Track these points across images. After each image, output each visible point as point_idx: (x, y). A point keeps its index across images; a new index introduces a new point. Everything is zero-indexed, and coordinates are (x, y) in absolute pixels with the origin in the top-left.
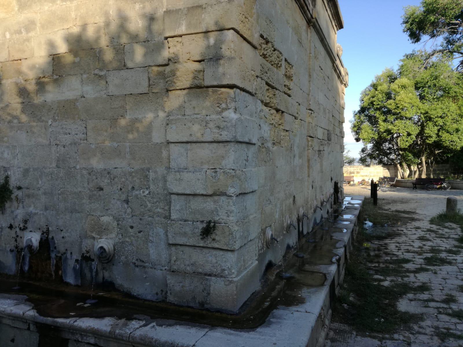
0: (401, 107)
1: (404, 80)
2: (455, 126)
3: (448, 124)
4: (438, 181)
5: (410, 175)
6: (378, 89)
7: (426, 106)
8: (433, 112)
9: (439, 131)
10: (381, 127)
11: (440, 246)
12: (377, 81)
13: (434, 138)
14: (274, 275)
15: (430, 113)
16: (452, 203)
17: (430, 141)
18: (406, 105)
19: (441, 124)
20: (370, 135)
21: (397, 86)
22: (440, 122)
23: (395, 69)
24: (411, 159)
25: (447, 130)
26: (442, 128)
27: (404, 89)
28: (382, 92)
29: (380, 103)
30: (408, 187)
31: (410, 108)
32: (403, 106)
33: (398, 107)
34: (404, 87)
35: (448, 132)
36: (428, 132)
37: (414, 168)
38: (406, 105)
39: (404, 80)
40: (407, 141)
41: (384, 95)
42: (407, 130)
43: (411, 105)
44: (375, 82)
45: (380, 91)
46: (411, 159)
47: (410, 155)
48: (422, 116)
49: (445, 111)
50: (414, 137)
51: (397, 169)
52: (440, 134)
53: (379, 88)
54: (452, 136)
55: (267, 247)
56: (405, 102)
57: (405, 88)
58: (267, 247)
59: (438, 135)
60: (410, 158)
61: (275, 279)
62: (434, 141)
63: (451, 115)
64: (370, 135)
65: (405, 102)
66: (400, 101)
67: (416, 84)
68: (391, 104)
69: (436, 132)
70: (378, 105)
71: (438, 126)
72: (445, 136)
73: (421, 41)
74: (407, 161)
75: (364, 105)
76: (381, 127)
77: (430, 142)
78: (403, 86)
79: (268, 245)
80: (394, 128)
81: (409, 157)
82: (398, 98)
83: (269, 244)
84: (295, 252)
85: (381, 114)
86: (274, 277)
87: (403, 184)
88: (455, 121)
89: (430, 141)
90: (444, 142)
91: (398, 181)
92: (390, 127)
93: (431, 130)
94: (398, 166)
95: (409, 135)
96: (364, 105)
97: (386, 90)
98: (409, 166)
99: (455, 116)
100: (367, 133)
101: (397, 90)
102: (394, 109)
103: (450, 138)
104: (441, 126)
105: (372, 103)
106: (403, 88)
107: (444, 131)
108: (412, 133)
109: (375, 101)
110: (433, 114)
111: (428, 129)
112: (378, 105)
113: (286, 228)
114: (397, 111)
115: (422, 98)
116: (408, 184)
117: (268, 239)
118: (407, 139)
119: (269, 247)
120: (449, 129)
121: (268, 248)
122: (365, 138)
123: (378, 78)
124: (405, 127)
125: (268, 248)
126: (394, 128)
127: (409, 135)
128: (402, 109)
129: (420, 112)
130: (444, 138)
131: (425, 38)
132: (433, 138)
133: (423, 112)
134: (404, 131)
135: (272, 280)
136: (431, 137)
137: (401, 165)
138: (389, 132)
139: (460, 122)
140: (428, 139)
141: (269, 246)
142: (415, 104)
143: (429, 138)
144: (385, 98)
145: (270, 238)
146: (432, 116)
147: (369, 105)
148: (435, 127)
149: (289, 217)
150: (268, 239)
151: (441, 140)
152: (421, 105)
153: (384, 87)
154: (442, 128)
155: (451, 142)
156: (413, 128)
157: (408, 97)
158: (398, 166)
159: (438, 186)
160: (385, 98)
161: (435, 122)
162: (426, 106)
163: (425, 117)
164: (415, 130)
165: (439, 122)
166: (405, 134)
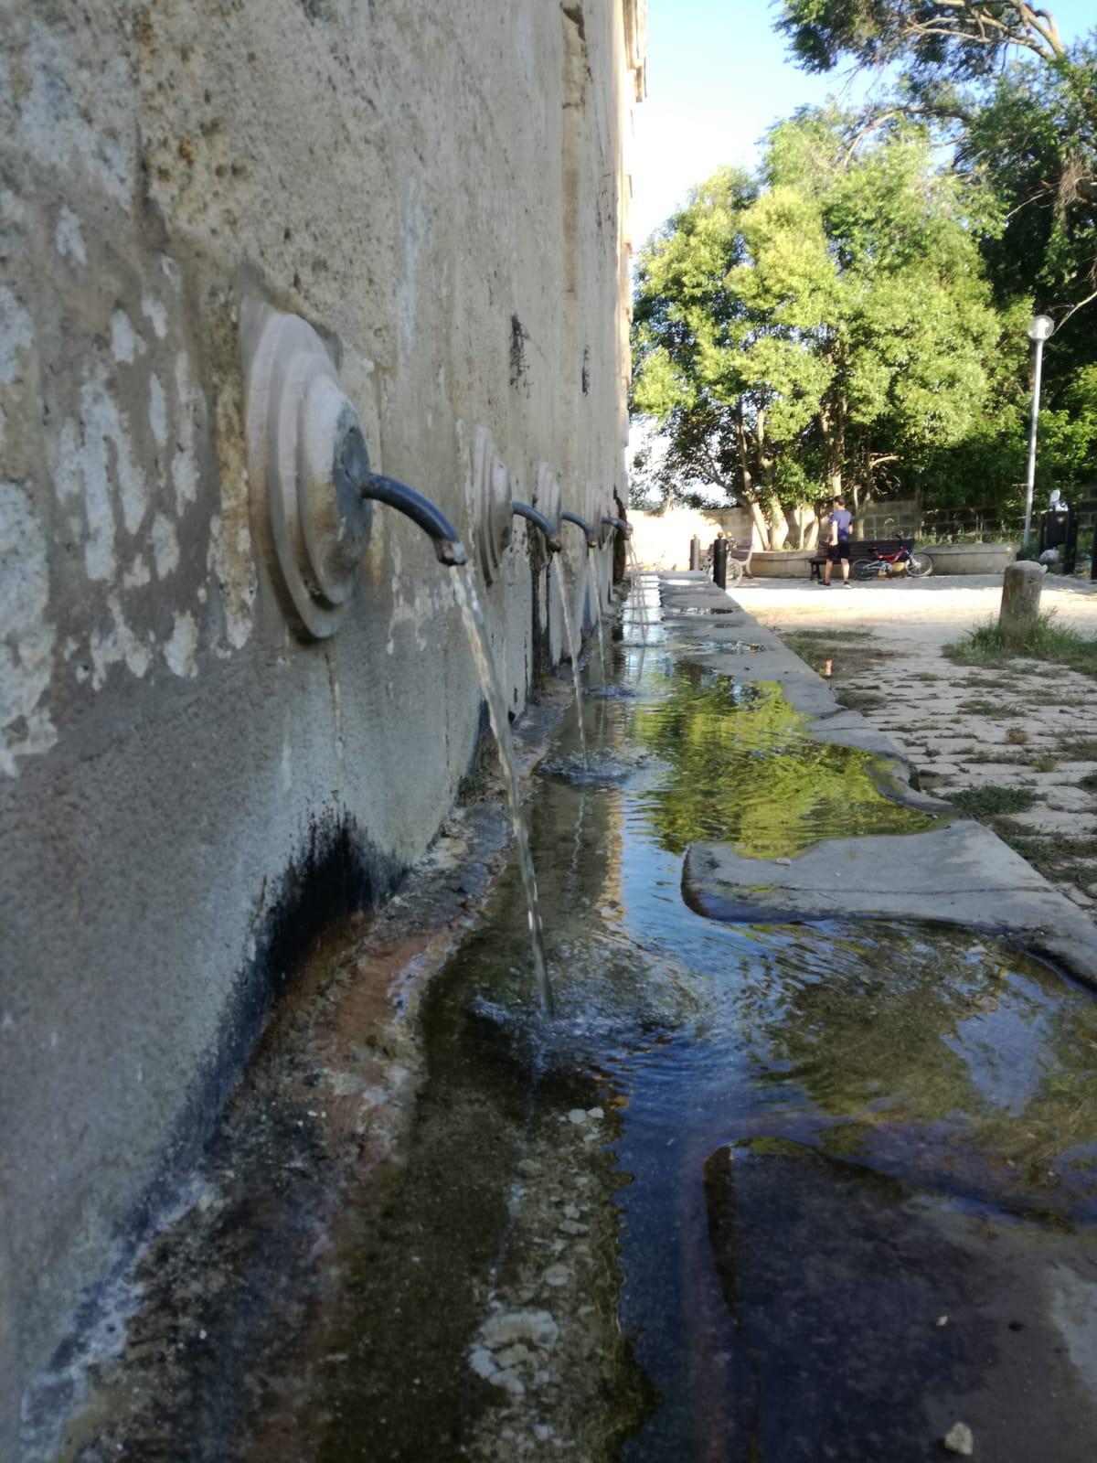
0: (776, 289)
1: (786, 197)
2: (946, 364)
3: (924, 357)
4: (900, 547)
5: (792, 539)
6: (699, 229)
7: (855, 294)
8: (881, 313)
9: (894, 380)
10: (707, 363)
11: (1087, 733)
12: (692, 203)
13: (879, 406)
14: (397, 1030)
15: (869, 314)
16: (1026, 585)
17: (864, 417)
18: (794, 281)
19: (903, 358)
20: (672, 393)
21: (763, 217)
22: (900, 351)
23: (750, 163)
24: (797, 484)
25: (921, 378)
26: (903, 372)
27: (786, 228)
28: (711, 239)
29: (703, 279)
30: (792, 577)
31: (807, 293)
32: (783, 288)
33: (767, 291)
34: (785, 219)
35: (925, 384)
36: (861, 383)
37: (805, 515)
38: (794, 284)
39: (786, 197)
40: (792, 416)
41: (717, 250)
42: (793, 376)
43: (811, 286)
44: (685, 207)
45: (704, 237)
46: (797, 484)
47: (796, 468)
48: (843, 327)
49: (916, 311)
50: (813, 400)
51: (752, 518)
52: (898, 391)
53: (701, 224)
54: (936, 397)
55: (289, 610)
56: (791, 273)
57: (787, 221)
58: (289, 610)
59: (891, 396)
60: (795, 479)
61: (425, 1102)
62: (879, 416)
63: (934, 329)
64: (672, 393)
65: (791, 273)
66: (774, 266)
67: (827, 213)
68: (741, 281)
69: (886, 384)
70: (699, 285)
71: (891, 365)
72: (912, 396)
73: (835, 70)
74: (784, 490)
75: (650, 289)
76: (707, 363)
77: (866, 420)
78: (784, 215)
79: (302, 595)
80: (752, 364)
81: (792, 475)
82: (767, 257)
83: (307, 570)
84: (542, 752)
85: (707, 318)
86: (398, 1075)
87: (776, 567)
88: (943, 348)
89: (864, 415)
90: (910, 417)
91: (758, 559)
92: (739, 361)
93: (870, 379)
94: (756, 507)
95: (798, 395)
96: (650, 289)
97: (725, 235)
98: (788, 509)
99: (945, 333)
100: (659, 386)
101: (764, 229)
102: (754, 297)
103: (930, 405)
104: (901, 365)
105: (677, 281)
106: (782, 226)
107: (910, 381)
108: (809, 388)
109: (686, 273)
110: (880, 318)
111: (860, 372)
112: (699, 285)
113: (479, 535)
114: (761, 302)
115: (847, 262)
116: (791, 567)
117: (289, 509)
118: (792, 409)
119: (321, 625)
120: (928, 373)
121: (306, 639)
122: (653, 401)
123: (697, 195)
124: (787, 364)
125: (306, 639)
126: (752, 364)
127: (798, 395)
128: (782, 298)
129: (837, 311)
130: (912, 406)
131: (846, 60)
132: (877, 404)
133: (847, 311)
134: (785, 380)
135: (385, 1138)
136: (867, 400)
137: (765, 507)
138: (735, 383)
139: (959, 352)
140: (858, 410)
141: (322, 602)
142: (824, 284)
143: (860, 406)
144: (720, 262)
145: (321, 461)
146: (876, 327)
147: (666, 288)
148: (883, 368)
149: (492, 446)
150: (286, 471)
151: (901, 413)
152: (839, 287)
153: (718, 222)
154: (903, 372)
155: (933, 417)
156: (813, 371)
157: (800, 254)
158: (756, 507)
159: (901, 566)
160: (720, 262)
161: (883, 352)
162: (855, 294)
163: (853, 332)
164: (818, 376)
165: (896, 351)
166: (787, 389)
